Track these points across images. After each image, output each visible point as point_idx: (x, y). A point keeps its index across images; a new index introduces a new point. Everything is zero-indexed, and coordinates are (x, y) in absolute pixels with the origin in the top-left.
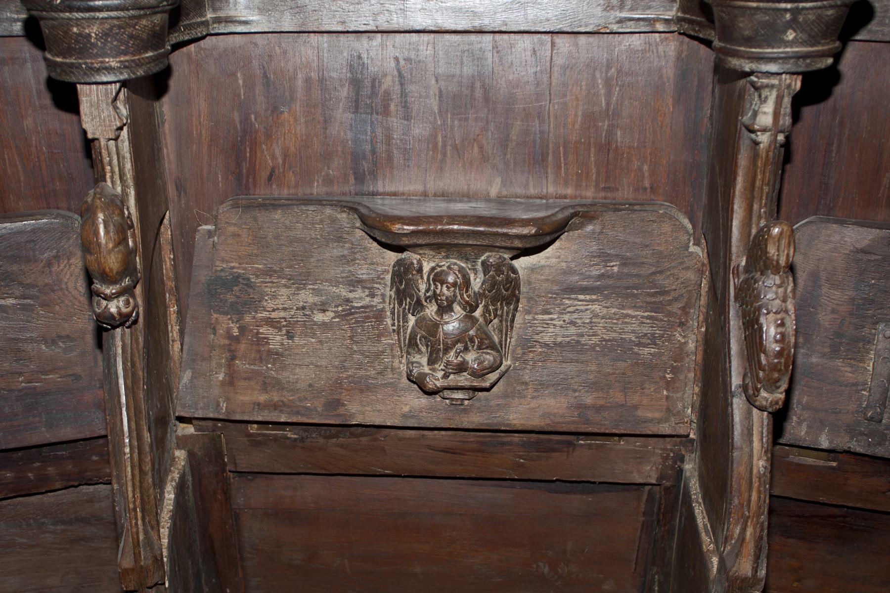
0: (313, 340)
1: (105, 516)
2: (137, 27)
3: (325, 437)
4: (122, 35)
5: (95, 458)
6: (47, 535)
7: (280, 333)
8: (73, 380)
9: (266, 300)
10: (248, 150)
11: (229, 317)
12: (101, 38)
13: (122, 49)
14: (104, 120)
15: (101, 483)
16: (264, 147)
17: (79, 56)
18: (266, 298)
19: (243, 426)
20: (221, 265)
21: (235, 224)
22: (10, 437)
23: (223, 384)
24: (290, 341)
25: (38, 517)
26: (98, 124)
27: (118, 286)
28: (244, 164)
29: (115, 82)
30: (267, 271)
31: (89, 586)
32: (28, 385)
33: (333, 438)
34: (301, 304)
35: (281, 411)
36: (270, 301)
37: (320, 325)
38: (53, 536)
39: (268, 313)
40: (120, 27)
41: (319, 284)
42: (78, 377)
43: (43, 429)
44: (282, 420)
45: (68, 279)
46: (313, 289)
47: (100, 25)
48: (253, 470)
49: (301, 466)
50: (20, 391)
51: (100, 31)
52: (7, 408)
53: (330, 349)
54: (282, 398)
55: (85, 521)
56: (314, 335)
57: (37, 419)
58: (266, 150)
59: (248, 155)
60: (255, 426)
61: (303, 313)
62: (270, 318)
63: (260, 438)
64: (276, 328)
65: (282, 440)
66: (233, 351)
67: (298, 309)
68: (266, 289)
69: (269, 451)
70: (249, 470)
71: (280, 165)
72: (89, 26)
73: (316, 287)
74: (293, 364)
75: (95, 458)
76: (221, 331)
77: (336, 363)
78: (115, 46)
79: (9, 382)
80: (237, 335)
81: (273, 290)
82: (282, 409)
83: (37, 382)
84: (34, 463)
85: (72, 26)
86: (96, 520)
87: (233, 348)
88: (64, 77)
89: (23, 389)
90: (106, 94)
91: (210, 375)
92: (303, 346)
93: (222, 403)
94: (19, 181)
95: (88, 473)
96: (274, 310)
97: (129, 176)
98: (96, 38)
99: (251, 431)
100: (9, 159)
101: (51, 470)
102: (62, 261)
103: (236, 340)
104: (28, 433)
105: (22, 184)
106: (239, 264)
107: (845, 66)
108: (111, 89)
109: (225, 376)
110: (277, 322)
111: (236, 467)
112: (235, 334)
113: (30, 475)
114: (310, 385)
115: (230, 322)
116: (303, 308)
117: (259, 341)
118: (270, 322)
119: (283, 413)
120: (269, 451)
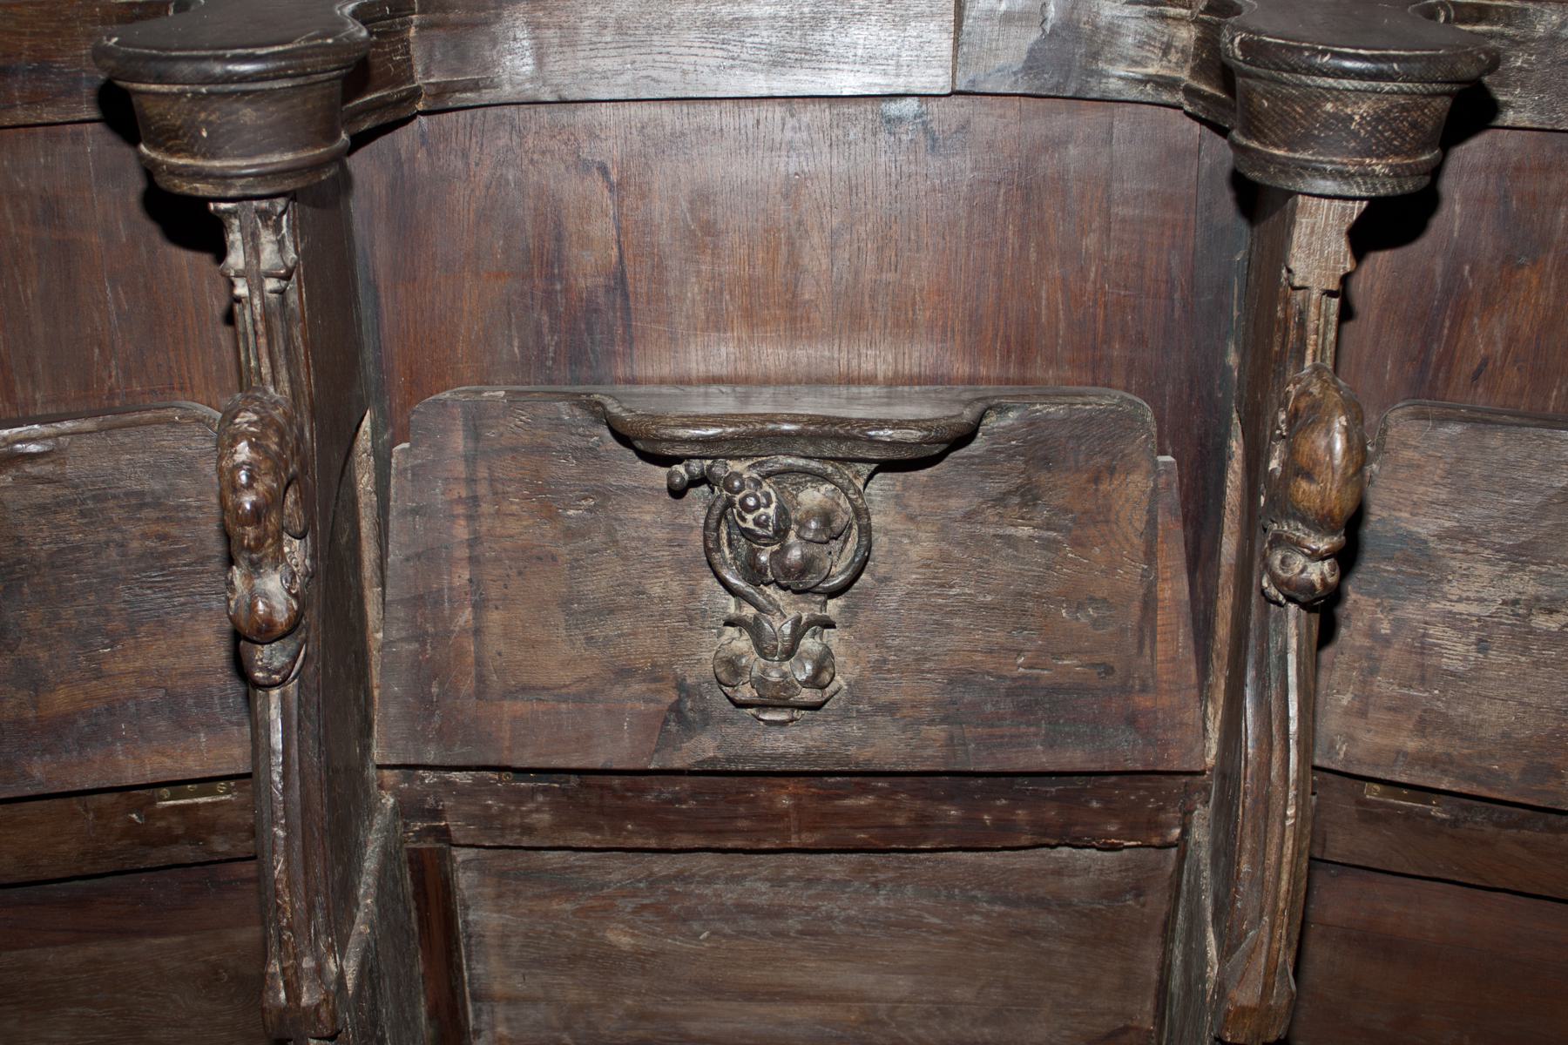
0: (1523, 659)
1: (1076, 900)
2: (1426, 111)
3: (1497, 824)
4: (1402, 122)
5: (1095, 804)
6: (976, 917)
7: (1464, 640)
8: (1099, 674)
9: (1449, 581)
10: (1447, 324)
11: (1378, 601)
12: (1369, 123)
13: (1395, 145)
14: (1327, 259)
15: (1093, 847)
16: (1476, 321)
17: (1321, 150)
18: (1450, 577)
19: (1357, 784)
20: (1379, 513)
21: (1416, 447)
22: (985, 753)
23: (1347, 712)
24: (1481, 656)
25: (969, 887)
26: (1316, 264)
27: (1336, 538)
28: (1435, 346)
29: (1361, 199)
30: (1460, 532)
31: (1018, 1011)
32: (1028, 671)
33: (1512, 828)
34: (1512, 595)
35: (1444, 772)
36: (1455, 584)
37: (1540, 634)
38: (984, 921)
39: (1449, 603)
40: (1404, 108)
41: (1551, 564)
42: (1109, 670)
43: (1039, 747)
44: (1443, 787)
45: (1123, 505)
46: (1540, 573)
47: (1375, 103)
48: (1351, 862)
49: (1441, 866)
50: (1014, 679)
51: (1371, 112)
52: (989, 706)
53: (1551, 678)
54: (1451, 750)
55: (1041, 903)
56: (1526, 650)
57: (1032, 729)
58: (1479, 327)
59: (1446, 331)
60: (1377, 787)
61: (1512, 611)
62: (1450, 612)
63: (1379, 810)
64: (1461, 630)
65: (1418, 818)
66: (1376, 659)
67: (1505, 603)
68: (1453, 563)
69: (1390, 833)
70: (1345, 861)
71: (1499, 355)
72: (1355, 103)
73: (1544, 570)
74: (1478, 694)
75: (1095, 804)
76: (1360, 624)
77: (1558, 703)
78: (1387, 139)
79: (1000, 663)
80: (1386, 634)
81: (1465, 565)
82: (1446, 767)
83: (1043, 669)
84: (999, 799)
85: (1328, 100)
86: (1060, 906)
87: (1376, 655)
88: (1281, 182)
89: (1019, 677)
90: (1343, 216)
91: (1327, 695)
92: (1501, 667)
93: (1340, 743)
94: (1057, 335)
95: (1078, 828)
96: (1460, 600)
97: (1328, 354)
98: (1359, 124)
99: (1368, 797)
100: (1048, 299)
101: (1021, 814)
102: (1117, 475)
103: (1386, 641)
104: (1014, 750)
105: (1060, 341)
106: (1411, 514)
107: (1450, 186)
108: (1353, 208)
109: (1353, 699)
110: (1462, 620)
111: (1323, 851)
112: (1383, 631)
113: (986, 817)
114: (1504, 735)
115: (1379, 610)
116: (1515, 602)
117: (1424, 649)
118: (1451, 619)
119: (1446, 776)
120: (1390, 833)
